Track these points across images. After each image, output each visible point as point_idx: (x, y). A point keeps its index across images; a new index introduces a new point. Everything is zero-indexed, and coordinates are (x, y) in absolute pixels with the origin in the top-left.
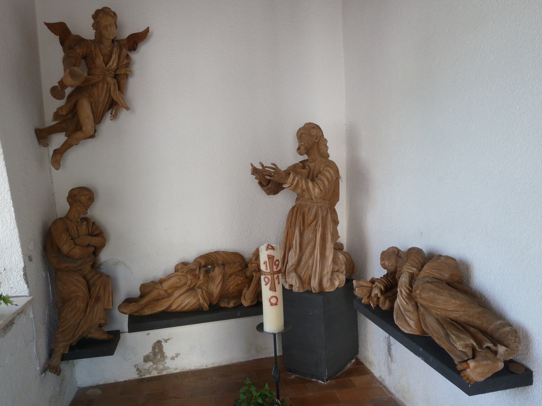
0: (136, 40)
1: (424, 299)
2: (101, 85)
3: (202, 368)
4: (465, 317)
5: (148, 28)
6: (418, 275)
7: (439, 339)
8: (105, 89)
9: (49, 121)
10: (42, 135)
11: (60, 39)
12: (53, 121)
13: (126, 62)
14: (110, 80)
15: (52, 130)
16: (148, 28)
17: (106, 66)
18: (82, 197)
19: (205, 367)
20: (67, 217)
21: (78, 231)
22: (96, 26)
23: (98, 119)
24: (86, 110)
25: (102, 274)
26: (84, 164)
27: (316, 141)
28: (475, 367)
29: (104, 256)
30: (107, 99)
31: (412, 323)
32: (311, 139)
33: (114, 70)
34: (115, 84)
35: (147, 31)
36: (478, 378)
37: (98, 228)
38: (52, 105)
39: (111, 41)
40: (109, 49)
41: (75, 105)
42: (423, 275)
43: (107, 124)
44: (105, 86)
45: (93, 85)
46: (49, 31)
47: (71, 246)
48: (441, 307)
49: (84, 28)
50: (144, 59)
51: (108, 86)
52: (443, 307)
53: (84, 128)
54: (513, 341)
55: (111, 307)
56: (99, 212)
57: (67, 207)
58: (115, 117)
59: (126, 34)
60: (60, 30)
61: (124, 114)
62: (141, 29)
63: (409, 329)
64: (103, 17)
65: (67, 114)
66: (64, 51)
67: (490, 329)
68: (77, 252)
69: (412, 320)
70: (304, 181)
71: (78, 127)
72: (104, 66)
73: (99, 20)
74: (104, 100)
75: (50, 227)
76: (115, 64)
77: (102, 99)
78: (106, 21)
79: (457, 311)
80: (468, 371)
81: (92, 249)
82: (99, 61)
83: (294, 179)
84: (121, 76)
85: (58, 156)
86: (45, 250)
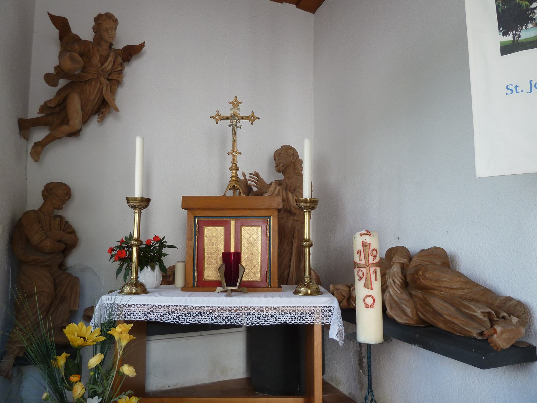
0: (132, 52)
1: (428, 279)
2: (94, 83)
3: (164, 389)
4: (471, 294)
5: (144, 43)
6: (408, 266)
7: (449, 315)
8: (97, 88)
9: (33, 113)
10: (25, 126)
11: (60, 33)
12: (39, 113)
13: (119, 68)
14: (103, 79)
15: (36, 123)
16: (144, 43)
17: (101, 66)
18: (58, 194)
19: (167, 388)
20: (41, 209)
21: (50, 226)
22: (97, 29)
23: (85, 121)
24: (75, 105)
25: (70, 275)
26: (65, 162)
27: (293, 161)
28: (502, 333)
29: (73, 260)
30: (97, 99)
31: (408, 311)
32: (287, 161)
33: (108, 73)
34: (107, 85)
35: (142, 45)
36: (505, 344)
37: (70, 226)
38: (41, 94)
39: (108, 45)
40: (106, 52)
41: (65, 100)
42: (414, 265)
43: (93, 127)
44: (98, 85)
45: (86, 82)
46: (51, 22)
47: (42, 236)
48: (446, 286)
49: (84, 30)
50: (135, 72)
51: (100, 86)
52: (447, 285)
53: (71, 122)
54: (523, 312)
55: (77, 309)
56: (72, 214)
57: (41, 201)
58: (101, 120)
59: (120, 45)
60: (61, 24)
61: (110, 120)
62: (136, 42)
63: (405, 318)
64: (105, 23)
65: (56, 107)
66: (62, 46)
67: (495, 305)
68: (48, 244)
69: (409, 307)
70: (284, 191)
71: (65, 121)
72: (100, 65)
73: (100, 22)
74: (95, 99)
75: (20, 219)
76: (110, 67)
77: (92, 98)
78: (106, 24)
79: (462, 289)
80: (495, 336)
81: (63, 246)
82: (96, 60)
83: (275, 189)
84: (115, 80)
85: (38, 150)
86: (11, 242)
